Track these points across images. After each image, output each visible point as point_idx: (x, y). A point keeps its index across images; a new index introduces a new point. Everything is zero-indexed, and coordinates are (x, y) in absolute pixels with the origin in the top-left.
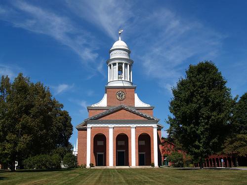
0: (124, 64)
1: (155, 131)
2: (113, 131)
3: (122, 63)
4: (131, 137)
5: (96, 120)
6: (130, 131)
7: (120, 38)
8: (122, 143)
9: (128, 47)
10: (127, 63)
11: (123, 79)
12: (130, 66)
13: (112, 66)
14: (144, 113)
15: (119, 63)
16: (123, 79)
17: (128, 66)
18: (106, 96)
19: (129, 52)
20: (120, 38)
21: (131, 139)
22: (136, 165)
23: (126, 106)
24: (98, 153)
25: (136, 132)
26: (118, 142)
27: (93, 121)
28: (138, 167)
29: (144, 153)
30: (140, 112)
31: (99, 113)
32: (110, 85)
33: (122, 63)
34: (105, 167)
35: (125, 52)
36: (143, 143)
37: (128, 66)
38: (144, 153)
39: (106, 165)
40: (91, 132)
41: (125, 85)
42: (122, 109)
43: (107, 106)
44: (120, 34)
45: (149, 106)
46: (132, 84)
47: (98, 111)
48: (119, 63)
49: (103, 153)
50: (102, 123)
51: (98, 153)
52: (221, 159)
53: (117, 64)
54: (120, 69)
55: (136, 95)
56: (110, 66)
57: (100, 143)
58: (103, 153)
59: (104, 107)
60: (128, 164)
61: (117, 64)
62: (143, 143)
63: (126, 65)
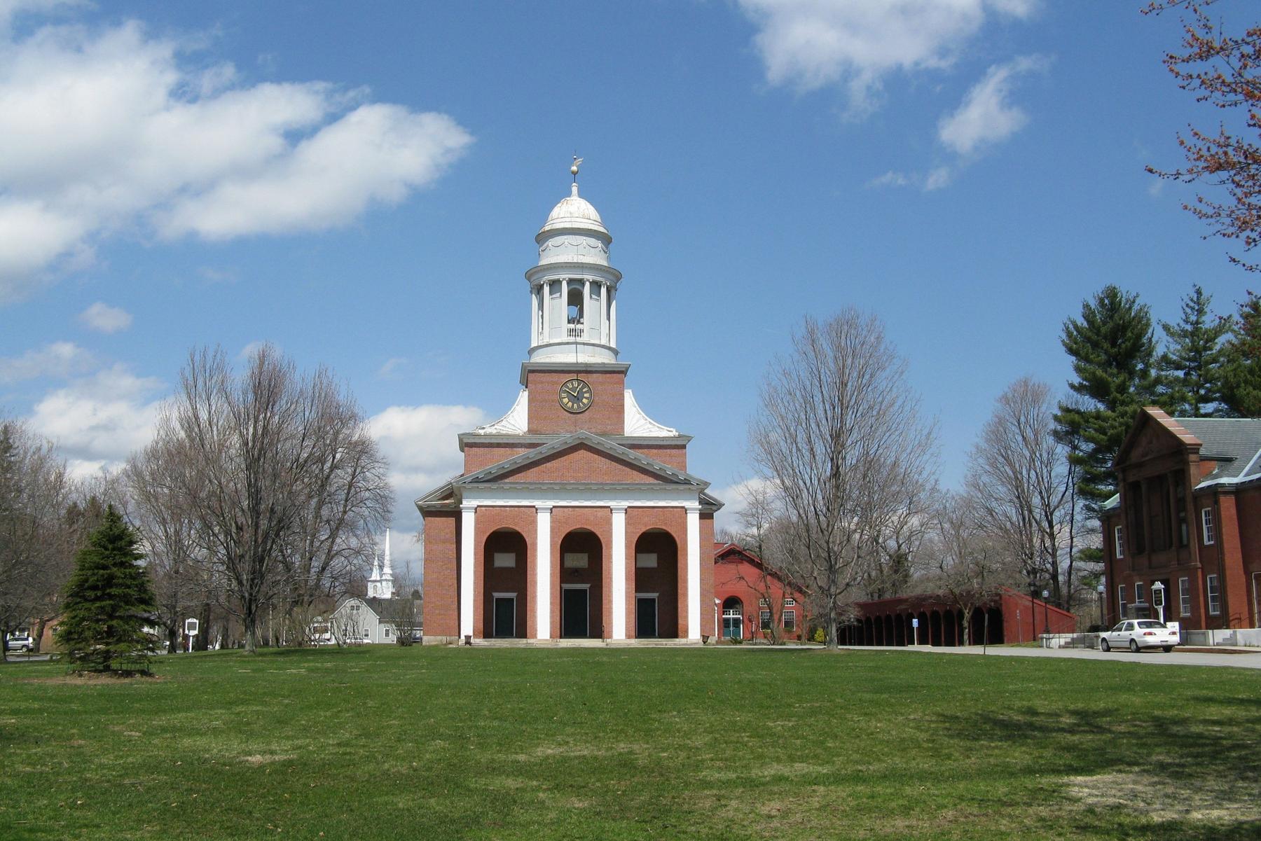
0: (587, 285)
1: (693, 521)
2: (551, 517)
3: (582, 282)
4: (535, 544)
5: (496, 479)
6: (534, 522)
7: (575, 189)
8: (580, 561)
9: (604, 222)
10: (598, 279)
11: (585, 338)
12: (608, 291)
13: (546, 289)
14: (656, 461)
15: (570, 282)
16: (585, 338)
17: (604, 291)
18: (524, 397)
19: (606, 240)
20: (575, 189)
21: (610, 547)
22: (628, 636)
23: (595, 440)
24: (497, 595)
25: (554, 522)
26: (638, 555)
27: (482, 486)
28: (479, 642)
29: (655, 595)
30: (632, 455)
31: (506, 459)
32: (541, 358)
33: (582, 282)
34: (521, 643)
35: (593, 241)
36: (651, 561)
37: (604, 291)
38: (655, 595)
39: (524, 636)
40: (477, 522)
41: (581, 360)
42: (581, 446)
43: (530, 431)
44: (575, 173)
45: (674, 433)
46: (615, 352)
47: (497, 451)
48: (570, 282)
49: (513, 595)
50: (505, 493)
51: (497, 595)
52: (911, 617)
53: (564, 284)
54: (575, 299)
55: (629, 398)
56: (539, 289)
57: (505, 560)
58: (513, 595)
59: (518, 436)
60: (598, 632)
61: (564, 284)
62: (651, 561)
63: (596, 286)
